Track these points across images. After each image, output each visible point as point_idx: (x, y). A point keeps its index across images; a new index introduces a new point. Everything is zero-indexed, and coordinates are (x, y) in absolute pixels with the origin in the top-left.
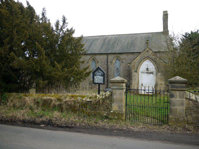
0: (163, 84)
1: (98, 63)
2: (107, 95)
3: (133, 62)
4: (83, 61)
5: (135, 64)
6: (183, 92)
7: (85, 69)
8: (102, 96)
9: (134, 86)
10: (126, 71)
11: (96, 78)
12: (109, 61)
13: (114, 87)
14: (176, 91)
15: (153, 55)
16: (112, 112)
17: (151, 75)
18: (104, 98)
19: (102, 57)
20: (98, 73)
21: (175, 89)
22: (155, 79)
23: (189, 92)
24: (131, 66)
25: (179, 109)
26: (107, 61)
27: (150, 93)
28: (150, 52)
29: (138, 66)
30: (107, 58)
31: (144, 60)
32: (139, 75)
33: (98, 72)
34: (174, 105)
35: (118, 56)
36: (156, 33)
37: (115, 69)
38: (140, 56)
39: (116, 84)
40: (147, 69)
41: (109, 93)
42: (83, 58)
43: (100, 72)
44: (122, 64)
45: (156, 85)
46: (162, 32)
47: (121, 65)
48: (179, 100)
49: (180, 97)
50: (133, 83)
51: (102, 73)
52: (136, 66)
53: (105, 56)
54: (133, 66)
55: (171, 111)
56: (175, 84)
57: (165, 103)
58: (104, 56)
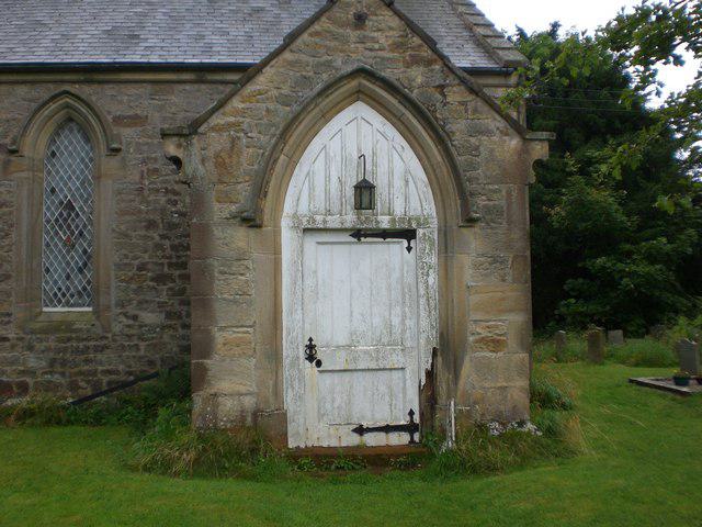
0: (512, 343)
3: (217, 120)
5: (234, 141)
9: (359, 95)
10: (151, 225)
15: (415, 61)
17: (397, 248)
22: (434, 293)
29: (270, 162)
31: (325, 103)
32: (277, 251)
37: (50, 211)
38: (292, 64)
40: (365, 192)
44: (110, 165)
45: (447, 351)
47: (98, 178)
50: (219, 337)
52: (248, 160)
54: (220, 164)
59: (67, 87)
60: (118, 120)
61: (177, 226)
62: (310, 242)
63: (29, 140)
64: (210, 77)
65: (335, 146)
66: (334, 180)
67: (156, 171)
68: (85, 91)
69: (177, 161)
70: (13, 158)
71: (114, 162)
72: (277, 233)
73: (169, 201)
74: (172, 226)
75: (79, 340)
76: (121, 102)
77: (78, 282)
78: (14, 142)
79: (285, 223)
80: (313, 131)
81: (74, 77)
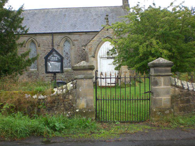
1: (39, 46)
2: (68, 88)
3: (89, 44)
4: (22, 42)
6: (169, 77)
7: (24, 55)
8: (61, 90)
10: (79, 56)
11: (49, 64)
12: (55, 44)
13: (80, 76)
14: (161, 77)
16: (77, 111)
18: (64, 92)
19: (44, 38)
20: (52, 58)
21: (159, 74)
23: (174, 77)
24: (87, 49)
25: (164, 99)
26: (53, 43)
27: (112, 83)
28: (111, 31)
29: (96, 49)
30: (53, 40)
32: (97, 60)
33: (53, 56)
34: (158, 95)
35: (67, 36)
36: (115, 6)
39: (82, 71)
41: (72, 85)
42: (22, 40)
43: (55, 56)
44: (74, 47)
46: (121, 6)
47: (71, 49)
48: (164, 88)
49: (165, 84)
51: (58, 57)
52: (93, 49)
53: (49, 38)
54: (90, 50)
55: (155, 102)
56: (159, 68)
57: (146, 93)
58: (48, 36)
59: (66, 36)
60: (74, 40)
61: (83, 56)
62: (102, 59)
63: (61, 44)
64: (87, 33)
65: (104, 47)
66: (105, 51)
67: (80, 48)
68: (69, 36)
69: (84, 49)
70: (59, 46)
71: (74, 47)
72: (97, 58)
73: (82, 52)
74: (82, 56)
75: (69, 73)
76: (74, 38)
77: (69, 64)
78: (59, 44)
79: (98, 57)
80: (102, 45)
81: (67, 34)
